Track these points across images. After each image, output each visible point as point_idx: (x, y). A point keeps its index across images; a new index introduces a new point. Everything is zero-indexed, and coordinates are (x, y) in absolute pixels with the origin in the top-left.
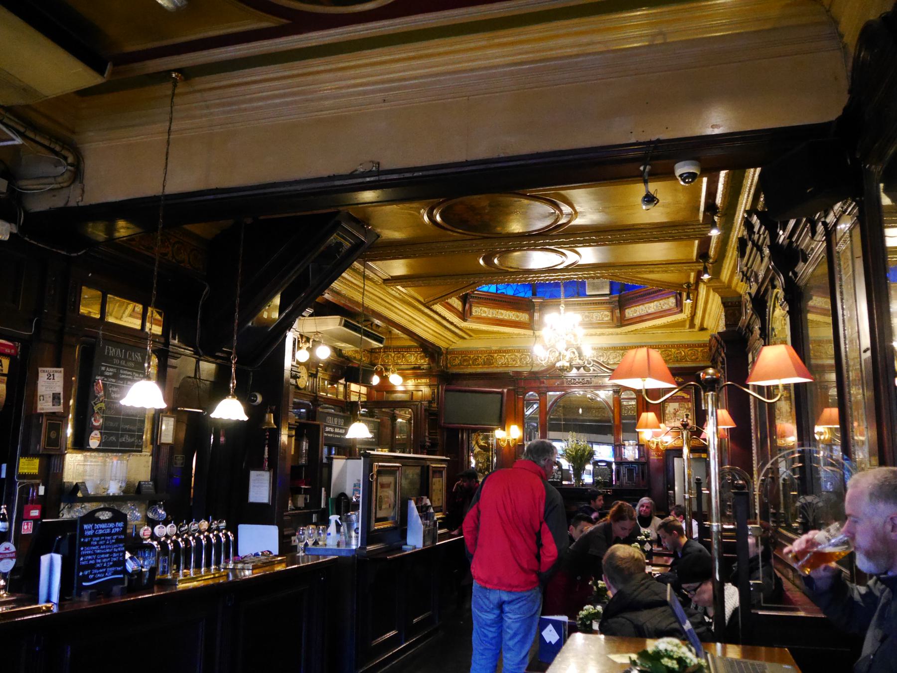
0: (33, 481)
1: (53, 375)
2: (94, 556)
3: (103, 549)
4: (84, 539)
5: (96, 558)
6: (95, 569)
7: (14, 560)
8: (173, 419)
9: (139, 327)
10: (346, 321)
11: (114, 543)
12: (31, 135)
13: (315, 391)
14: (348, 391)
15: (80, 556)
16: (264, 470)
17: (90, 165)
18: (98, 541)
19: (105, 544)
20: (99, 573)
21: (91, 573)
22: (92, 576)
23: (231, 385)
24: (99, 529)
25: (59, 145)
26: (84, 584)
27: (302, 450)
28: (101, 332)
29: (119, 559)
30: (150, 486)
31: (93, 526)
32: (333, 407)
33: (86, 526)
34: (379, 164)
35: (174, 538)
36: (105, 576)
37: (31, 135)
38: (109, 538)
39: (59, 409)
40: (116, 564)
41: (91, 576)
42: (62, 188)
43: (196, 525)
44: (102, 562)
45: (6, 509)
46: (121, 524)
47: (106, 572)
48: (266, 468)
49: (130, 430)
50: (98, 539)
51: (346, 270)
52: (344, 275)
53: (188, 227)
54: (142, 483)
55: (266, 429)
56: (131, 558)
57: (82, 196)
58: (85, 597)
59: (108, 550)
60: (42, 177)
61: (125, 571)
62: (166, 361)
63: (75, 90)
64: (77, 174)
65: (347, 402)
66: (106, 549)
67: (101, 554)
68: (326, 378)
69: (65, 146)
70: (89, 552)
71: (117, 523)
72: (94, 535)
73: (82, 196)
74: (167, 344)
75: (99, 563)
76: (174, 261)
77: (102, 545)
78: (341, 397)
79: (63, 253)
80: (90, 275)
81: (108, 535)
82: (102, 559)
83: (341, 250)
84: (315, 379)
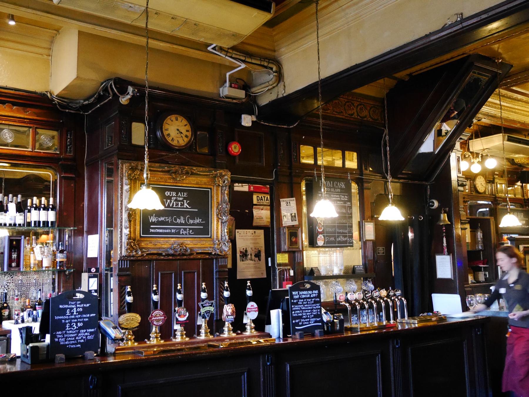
0: (286, 268)
1: (290, 202)
2: (301, 311)
3: (306, 307)
4: (294, 300)
5: (302, 312)
6: (302, 319)
7: (257, 312)
8: (372, 223)
9: (341, 166)
10: (508, 136)
11: (313, 304)
12: (249, 60)
13: (494, 194)
14: (525, 191)
15: (292, 311)
16: (444, 255)
17: (288, 69)
18: (302, 302)
19: (307, 304)
20: (306, 322)
21: (300, 322)
22: (301, 323)
23: (390, 197)
24: (303, 294)
25: (266, 61)
26: (296, 328)
27: (478, 239)
28: (315, 172)
29: (317, 313)
30: (361, 268)
31: (299, 293)
32: (514, 204)
33: (294, 293)
34: (462, 14)
35: (361, 301)
36: (309, 324)
37: (249, 60)
38: (309, 300)
39: (296, 223)
40: (315, 316)
41: (300, 323)
42: (274, 87)
43: (377, 293)
44: (306, 315)
45: (250, 283)
46: (317, 292)
47: (310, 321)
48: (446, 253)
49: (343, 233)
50: (302, 300)
51: (491, 95)
52: (490, 100)
53: (358, 91)
54: (355, 267)
55: (442, 225)
56: (325, 313)
57: (284, 90)
58: (297, 334)
59: (309, 308)
60: (263, 84)
61: (322, 321)
62: (362, 185)
63: (262, 24)
64: (280, 77)
65: (524, 199)
66: (308, 306)
67: (306, 310)
68: (503, 182)
69: (270, 61)
70: (298, 308)
71: (314, 291)
72: (300, 298)
73: (284, 90)
74: (361, 174)
75: (304, 315)
76: (359, 117)
77: (306, 304)
78: (519, 196)
79: (285, 127)
80: (304, 137)
81: (309, 298)
82: (306, 313)
83: (480, 83)
84: (493, 184)
